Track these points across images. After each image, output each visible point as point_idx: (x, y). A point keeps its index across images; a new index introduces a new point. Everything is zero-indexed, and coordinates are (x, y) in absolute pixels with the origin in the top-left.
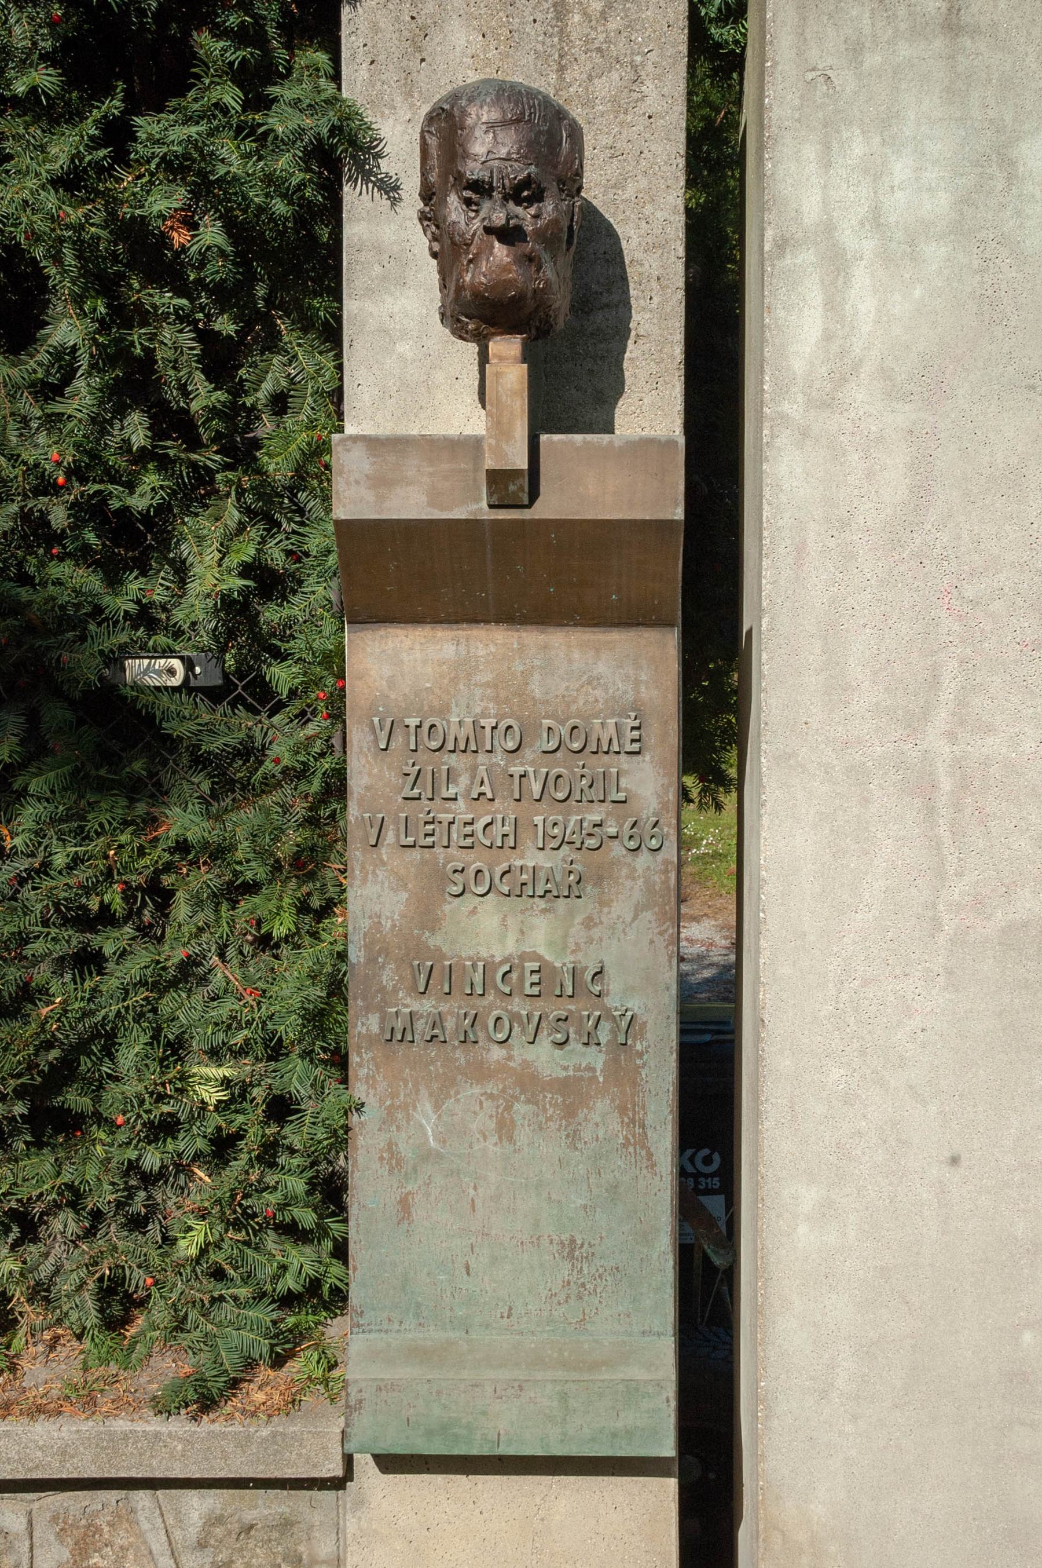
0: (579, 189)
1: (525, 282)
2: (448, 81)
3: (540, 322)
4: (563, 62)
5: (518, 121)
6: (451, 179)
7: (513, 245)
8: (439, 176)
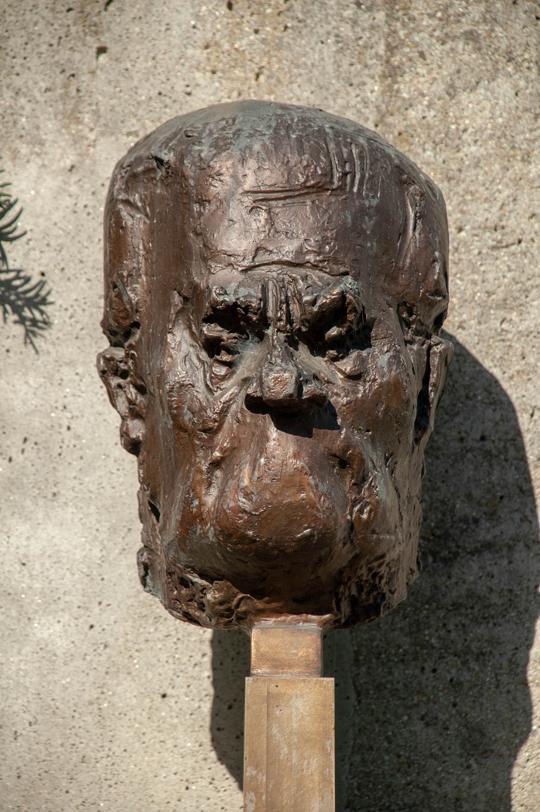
0: (440, 320)
1: (331, 510)
2: (154, 93)
3: (360, 589)
4: (396, 60)
5: (319, 188)
6: (177, 299)
7: (309, 434)
8: (149, 292)
